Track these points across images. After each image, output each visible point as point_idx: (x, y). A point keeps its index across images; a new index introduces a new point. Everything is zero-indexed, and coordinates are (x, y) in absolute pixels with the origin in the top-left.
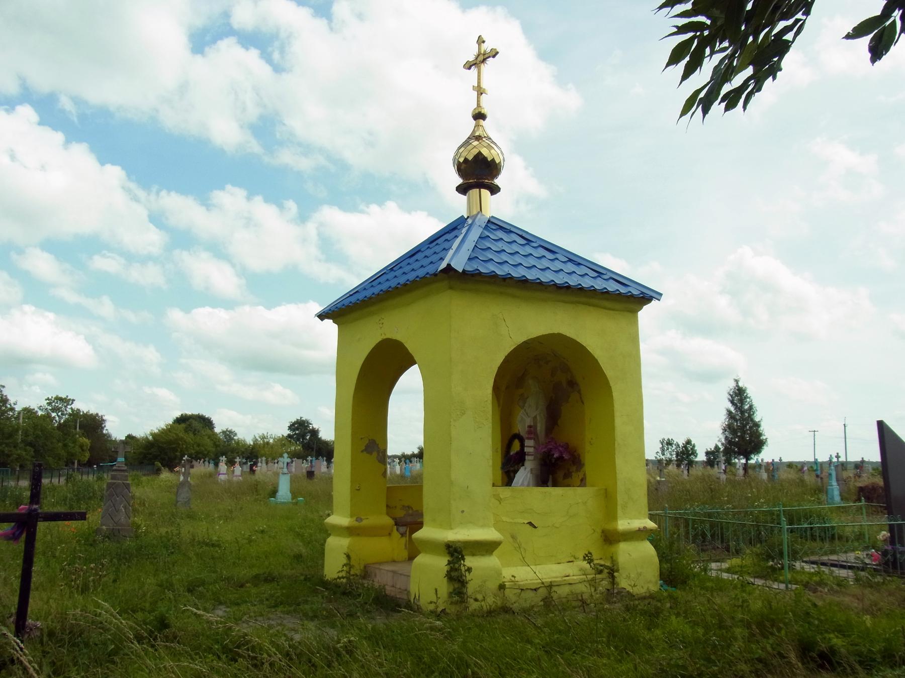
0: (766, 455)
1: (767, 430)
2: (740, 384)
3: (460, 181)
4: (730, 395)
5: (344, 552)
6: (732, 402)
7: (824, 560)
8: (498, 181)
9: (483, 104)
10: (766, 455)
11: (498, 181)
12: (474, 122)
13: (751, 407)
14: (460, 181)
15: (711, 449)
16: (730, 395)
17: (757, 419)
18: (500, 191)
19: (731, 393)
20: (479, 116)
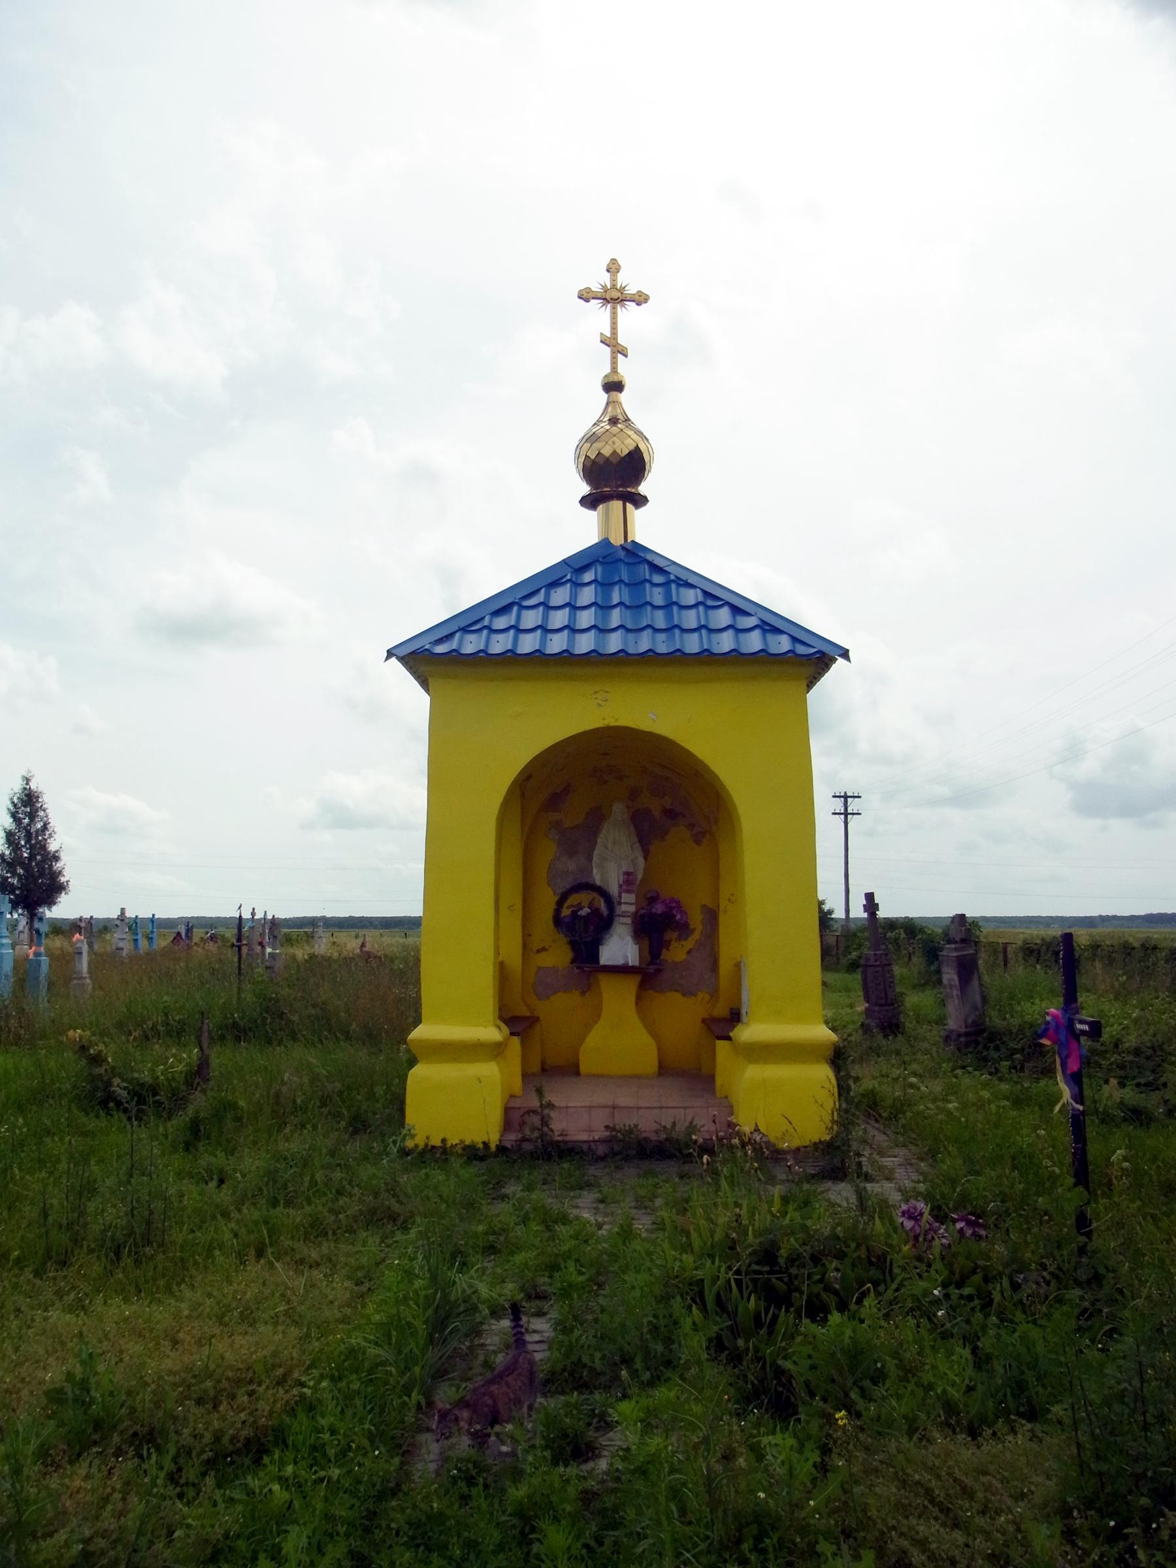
0: (63, 909)
1: (70, 868)
2: (33, 785)
3: (585, 489)
4: (13, 802)
5: (448, 1137)
6: (14, 815)
7: (571, 1142)
8: (643, 488)
9: (621, 370)
10: (63, 909)
11: (643, 488)
12: (606, 396)
13: (45, 827)
14: (585, 489)
15: (253, 914)
16: (13, 802)
17: (52, 847)
18: (645, 505)
19: (15, 800)
20: (613, 386)
